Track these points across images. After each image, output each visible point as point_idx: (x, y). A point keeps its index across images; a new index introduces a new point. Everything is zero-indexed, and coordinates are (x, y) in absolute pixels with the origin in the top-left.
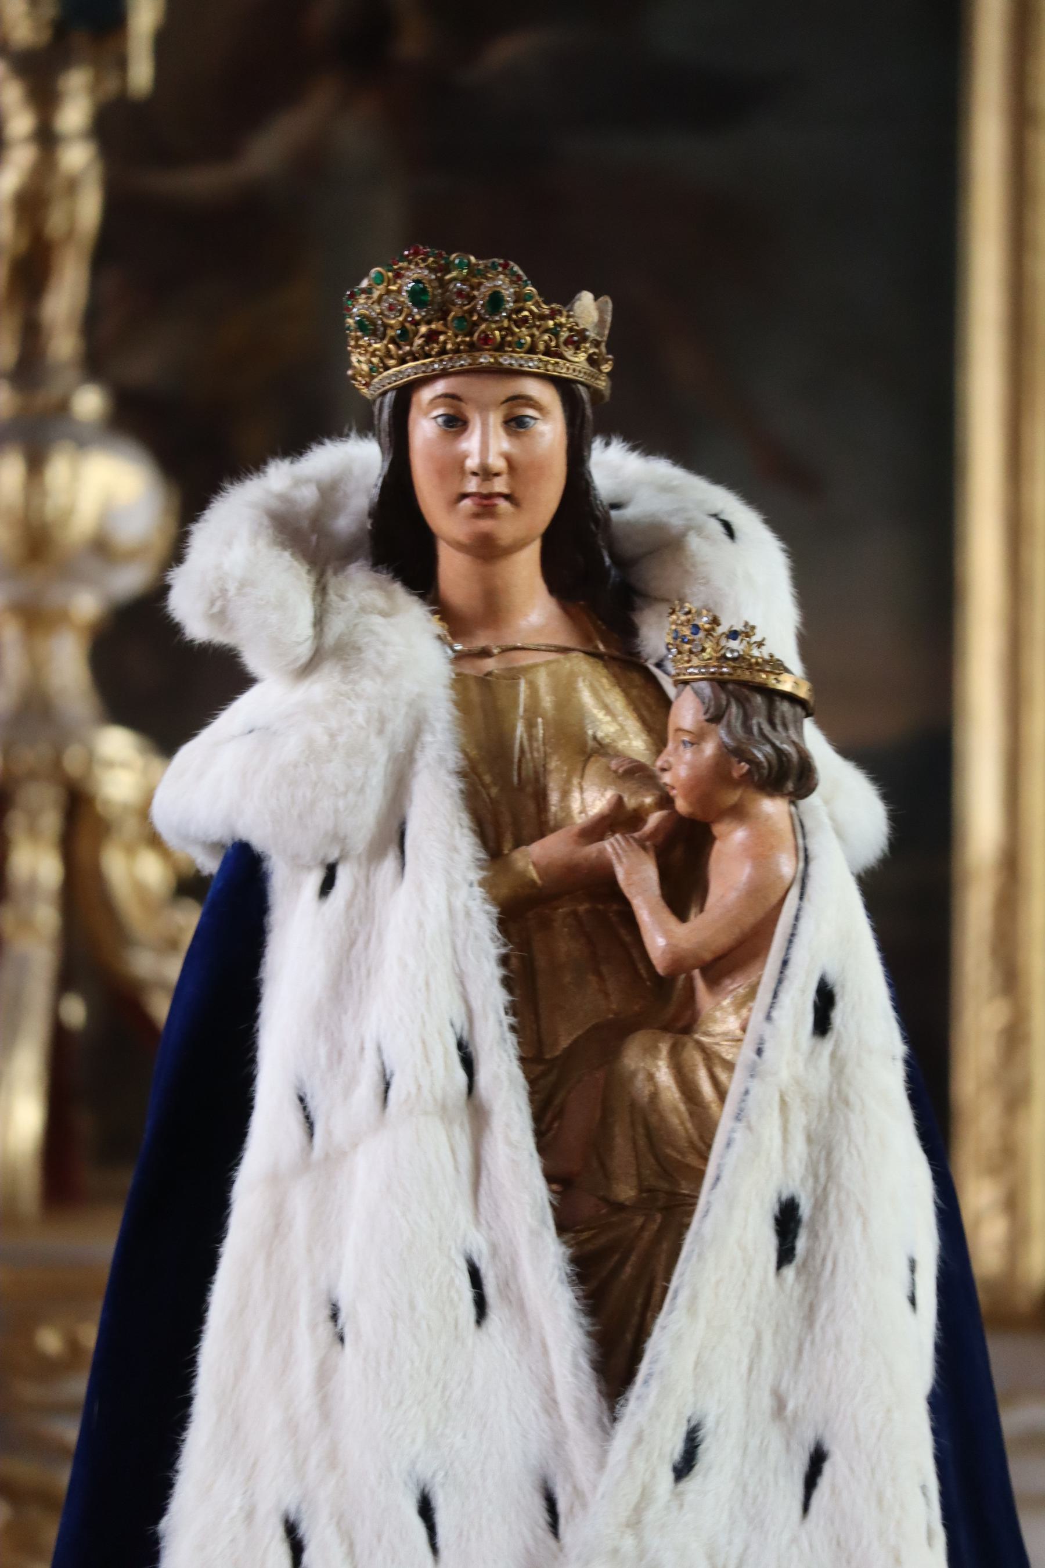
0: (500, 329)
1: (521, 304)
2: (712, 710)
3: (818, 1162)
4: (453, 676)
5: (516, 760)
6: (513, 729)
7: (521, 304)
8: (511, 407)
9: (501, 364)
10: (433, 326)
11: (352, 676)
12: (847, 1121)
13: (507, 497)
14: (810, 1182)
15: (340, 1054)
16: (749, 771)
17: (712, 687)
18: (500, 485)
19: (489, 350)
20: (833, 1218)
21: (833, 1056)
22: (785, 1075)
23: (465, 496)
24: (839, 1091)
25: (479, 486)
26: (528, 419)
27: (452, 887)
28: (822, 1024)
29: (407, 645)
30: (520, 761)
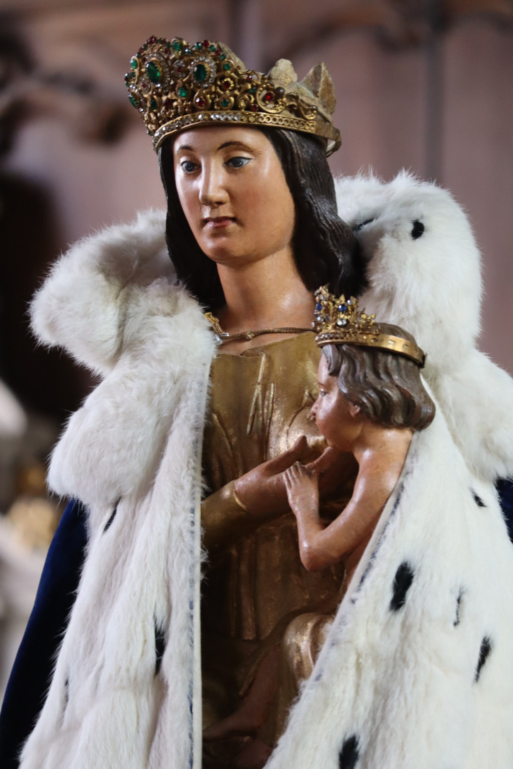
0: (211, 93)
1: (222, 73)
2: (332, 367)
3: (377, 710)
4: (215, 356)
5: (251, 415)
6: (252, 392)
7: (222, 73)
8: (227, 152)
9: (211, 119)
10: (169, 96)
11: (137, 362)
12: (403, 674)
13: (234, 219)
14: (370, 723)
15: (92, 646)
16: (361, 412)
17: (333, 349)
18: (225, 211)
19: (204, 110)
20: (379, 752)
21: (403, 624)
22: (361, 641)
23: (205, 221)
24: (402, 652)
25: (211, 213)
26: (243, 160)
27: (174, 514)
28: (398, 602)
29: (184, 338)
30: (254, 416)
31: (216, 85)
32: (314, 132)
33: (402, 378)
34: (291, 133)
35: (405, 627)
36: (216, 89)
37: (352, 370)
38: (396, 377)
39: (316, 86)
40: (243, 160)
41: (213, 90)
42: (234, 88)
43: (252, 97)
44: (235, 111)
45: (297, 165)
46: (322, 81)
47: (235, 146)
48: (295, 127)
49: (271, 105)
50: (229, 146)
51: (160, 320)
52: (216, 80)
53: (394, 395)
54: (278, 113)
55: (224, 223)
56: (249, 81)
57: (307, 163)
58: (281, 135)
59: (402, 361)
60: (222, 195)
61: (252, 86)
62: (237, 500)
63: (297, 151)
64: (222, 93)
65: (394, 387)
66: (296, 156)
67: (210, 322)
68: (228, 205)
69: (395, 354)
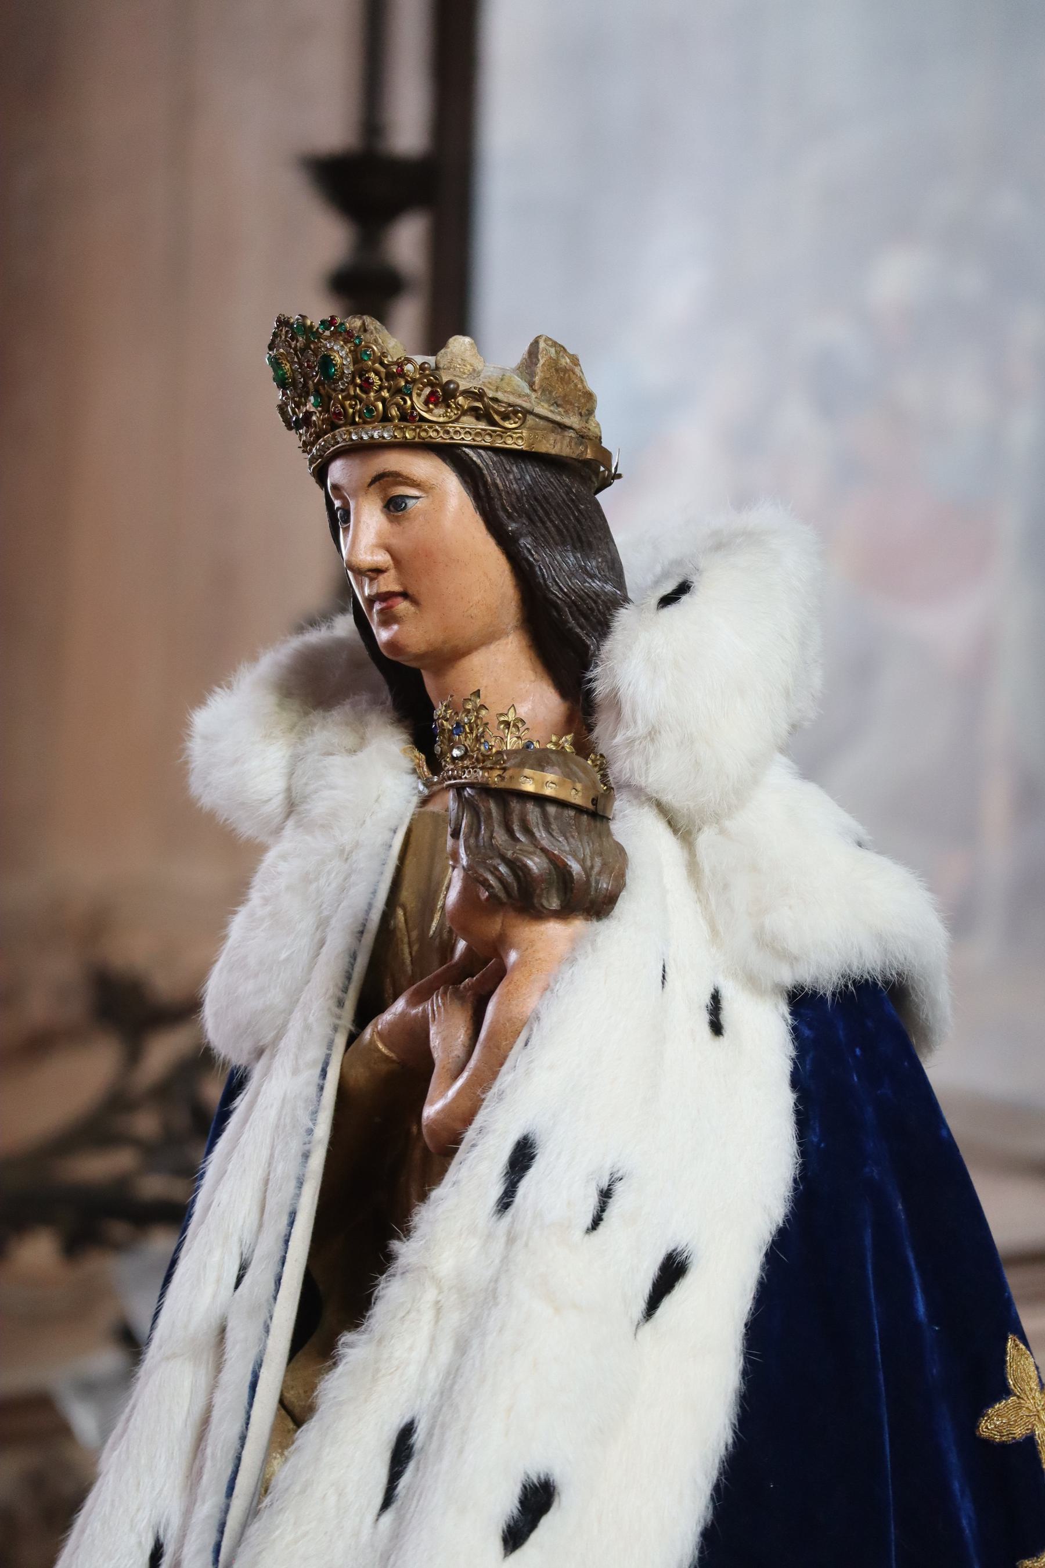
1: (360, 366)
7: (360, 366)
8: (384, 490)
13: (405, 595)
18: (388, 583)
20: (434, 1446)
31: (356, 385)
32: (524, 447)
33: (553, 836)
34: (481, 451)
35: (511, 1239)
36: (355, 391)
37: (474, 830)
38: (541, 834)
39: (533, 374)
40: (407, 501)
41: (352, 393)
42: (381, 388)
43: (407, 398)
44: (386, 424)
45: (497, 504)
46: (540, 365)
47: (390, 479)
48: (488, 441)
49: (440, 411)
50: (383, 479)
51: (338, 761)
52: (353, 374)
53: (535, 864)
54: (452, 422)
55: (390, 602)
56: (402, 374)
57: (518, 499)
58: (463, 455)
59: (552, 810)
60: (382, 558)
61: (407, 382)
62: (380, 1046)
63: (493, 480)
64: (364, 396)
65: (538, 851)
66: (492, 489)
67: (412, 761)
68: (392, 573)
69: (540, 800)
